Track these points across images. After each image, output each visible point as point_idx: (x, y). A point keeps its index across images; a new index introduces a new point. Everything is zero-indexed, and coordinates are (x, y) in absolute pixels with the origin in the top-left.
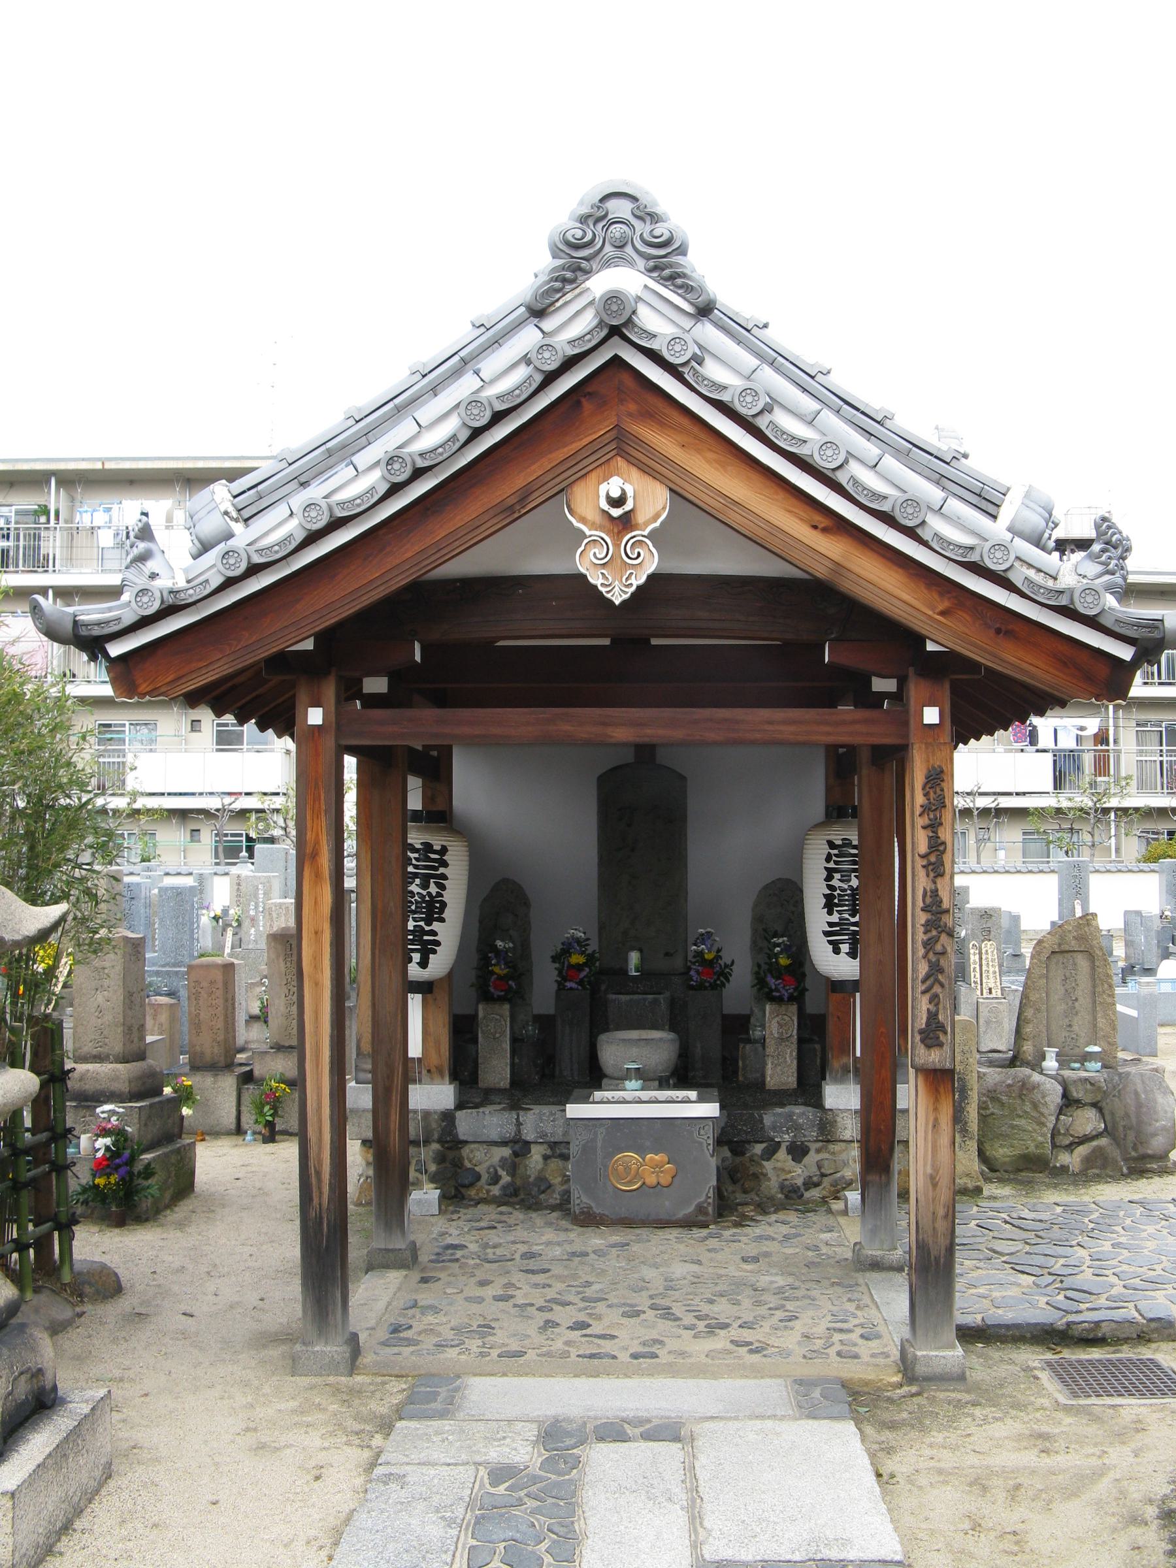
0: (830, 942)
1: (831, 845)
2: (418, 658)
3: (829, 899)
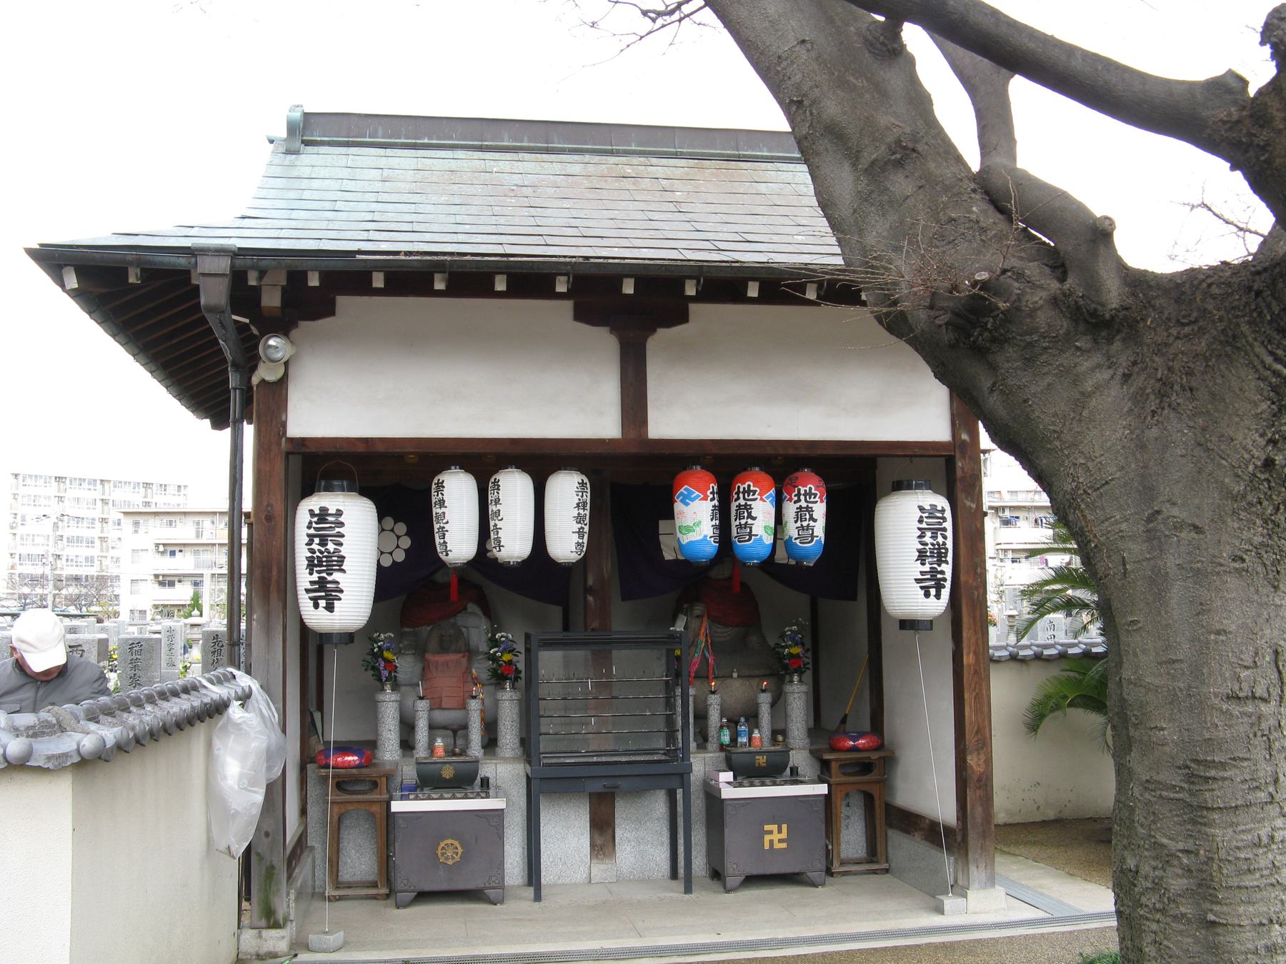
0: (311, 599)
1: (921, 509)
2: (882, 19)
3: (310, 560)
